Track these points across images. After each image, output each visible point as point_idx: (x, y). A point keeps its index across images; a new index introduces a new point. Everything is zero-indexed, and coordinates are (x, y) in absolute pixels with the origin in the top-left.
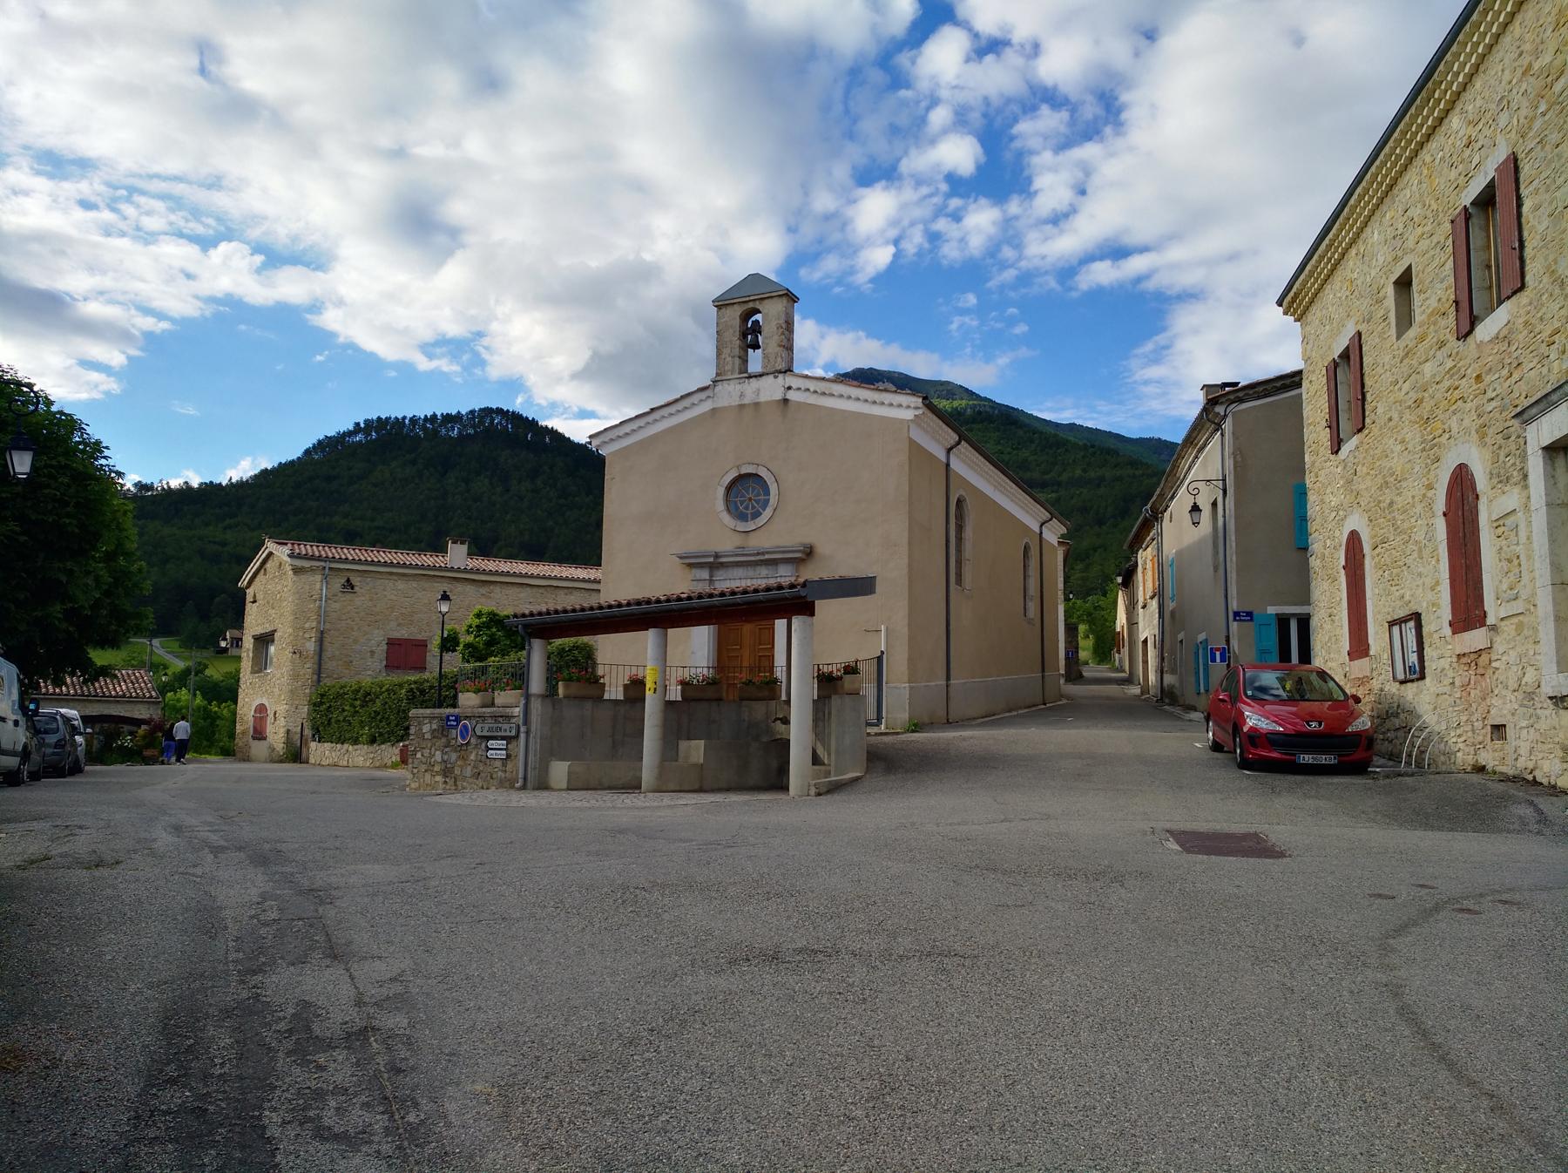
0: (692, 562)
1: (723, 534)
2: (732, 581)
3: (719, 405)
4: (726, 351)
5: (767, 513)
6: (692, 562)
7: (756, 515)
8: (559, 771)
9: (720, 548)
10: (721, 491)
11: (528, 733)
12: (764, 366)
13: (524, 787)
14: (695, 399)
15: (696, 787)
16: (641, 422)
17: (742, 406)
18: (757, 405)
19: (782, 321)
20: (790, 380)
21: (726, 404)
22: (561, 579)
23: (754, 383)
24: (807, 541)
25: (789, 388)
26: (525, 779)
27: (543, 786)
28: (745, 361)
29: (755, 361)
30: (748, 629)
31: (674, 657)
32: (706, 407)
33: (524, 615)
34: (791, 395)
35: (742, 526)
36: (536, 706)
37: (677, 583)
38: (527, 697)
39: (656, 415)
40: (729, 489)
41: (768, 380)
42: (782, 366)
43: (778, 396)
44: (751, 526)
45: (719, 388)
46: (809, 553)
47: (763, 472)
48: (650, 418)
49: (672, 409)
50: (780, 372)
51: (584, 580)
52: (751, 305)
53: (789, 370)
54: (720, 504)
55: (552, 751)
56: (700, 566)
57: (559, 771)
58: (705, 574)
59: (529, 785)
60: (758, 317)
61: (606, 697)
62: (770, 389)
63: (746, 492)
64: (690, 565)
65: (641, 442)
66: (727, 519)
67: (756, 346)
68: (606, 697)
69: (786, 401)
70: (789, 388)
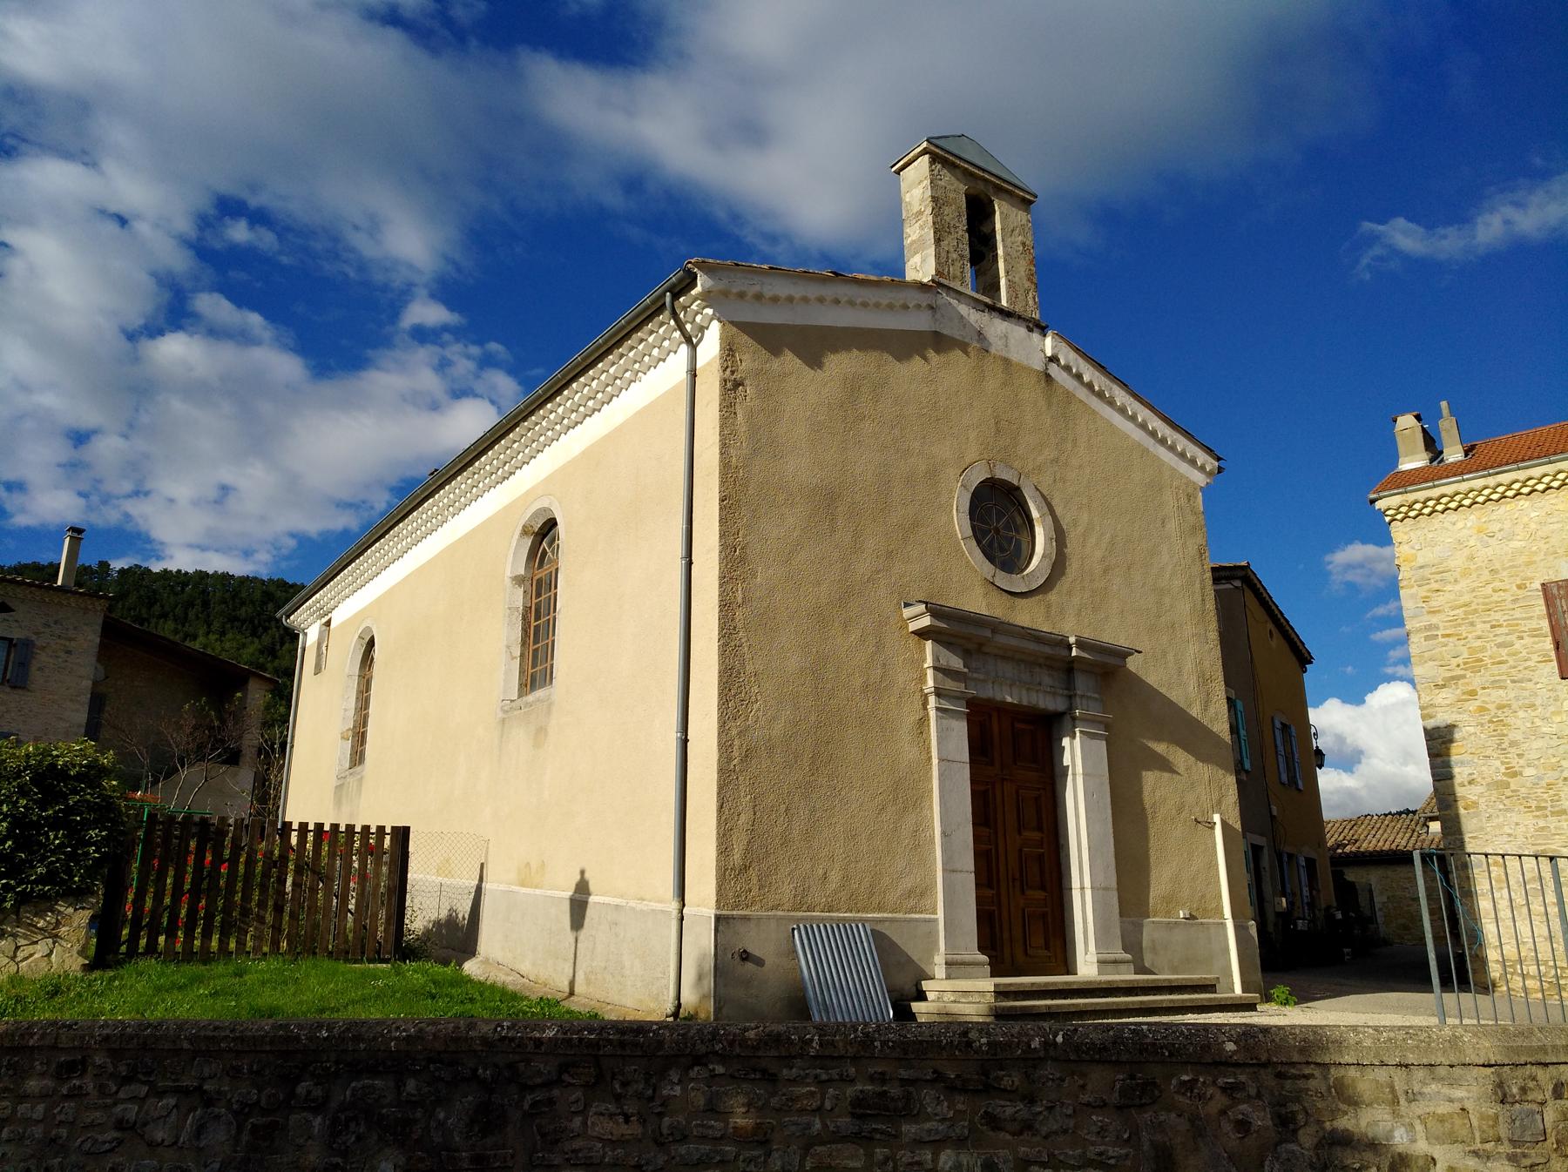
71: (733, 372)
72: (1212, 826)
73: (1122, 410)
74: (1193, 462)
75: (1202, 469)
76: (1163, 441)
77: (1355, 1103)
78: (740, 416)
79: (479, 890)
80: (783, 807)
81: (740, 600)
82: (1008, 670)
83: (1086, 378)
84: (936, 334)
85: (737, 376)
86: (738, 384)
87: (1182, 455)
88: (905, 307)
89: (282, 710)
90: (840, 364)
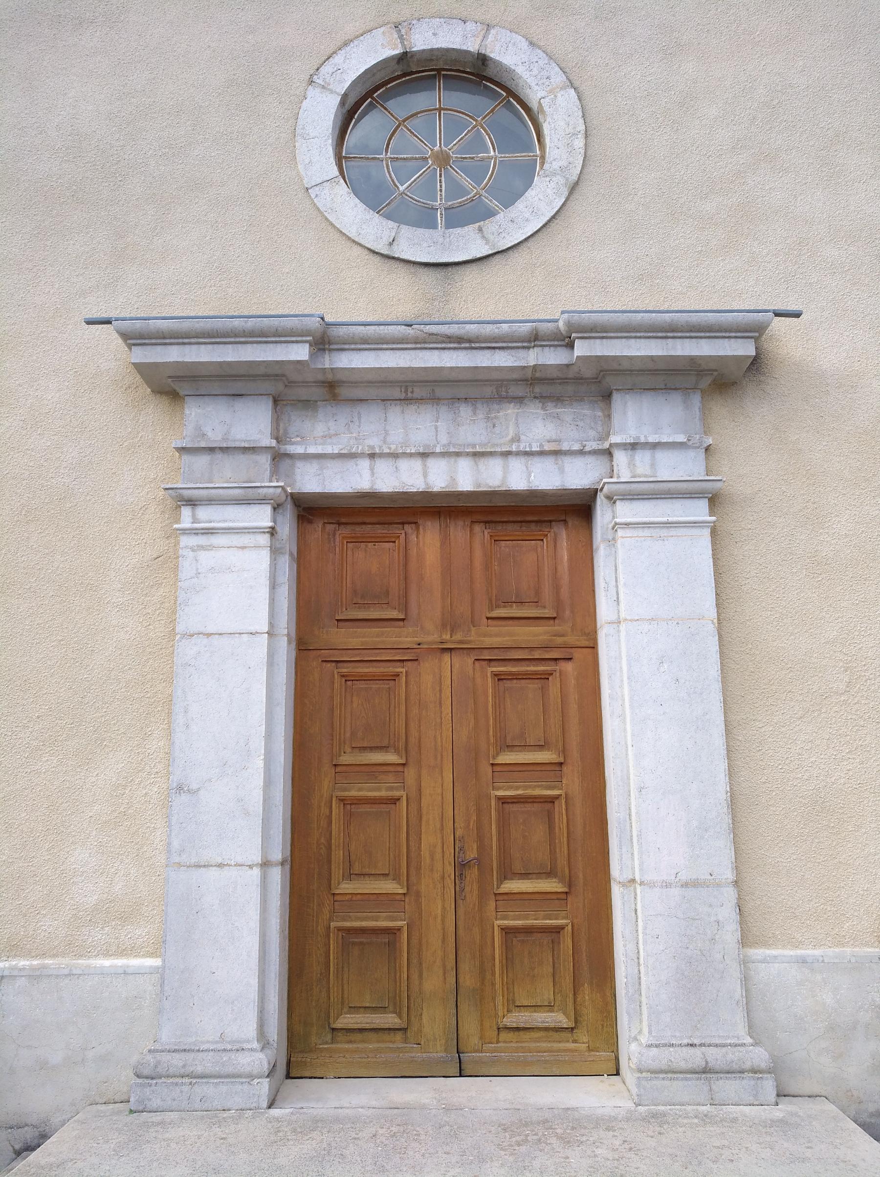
10: (321, 111)
35: (417, 245)
40: (351, 112)
44: (468, 243)
54: (317, 156)
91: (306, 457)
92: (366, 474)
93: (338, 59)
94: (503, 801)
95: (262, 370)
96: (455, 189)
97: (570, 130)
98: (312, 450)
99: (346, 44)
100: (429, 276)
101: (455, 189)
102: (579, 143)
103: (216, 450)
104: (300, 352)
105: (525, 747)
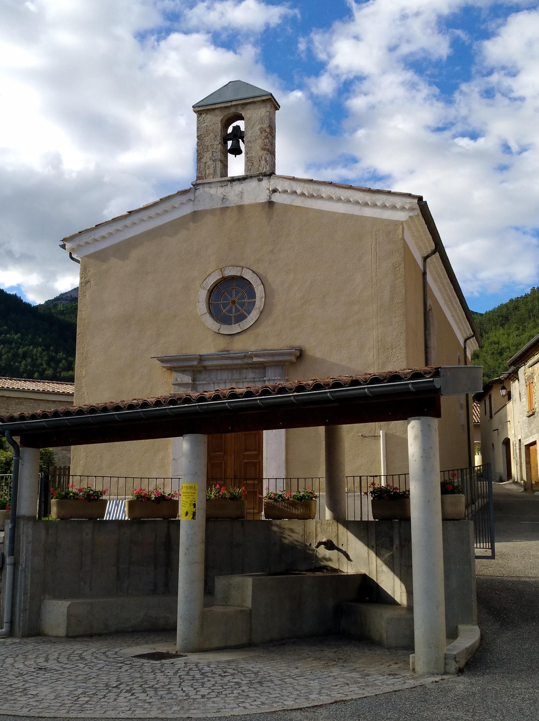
0: (175, 364)
1: (205, 337)
2: (215, 386)
3: (200, 208)
4: (207, 156)
5: (254, 316)
6: (175, 364)
7: (241, 318)
8: (57, 612)
9: (204, 351)
10: (203, 295)
11: (15, 565)
12: (247, 169)
13: (11, 634)
14: (176, 202)
15: (244, 640)
16: (119, 225)
17: (224, 210)
18: (240, 208)
19: (265, 125)
20: (273, 183)
21: (207, 207)
22: (13, 390)
23: (238, 187)
24: (298, 343)
25: (275, 191)
26: (12, 623)
27: (35, 632)
28: (225, 166)
29: (236, 166)
30: (231, 439)
31: (352, 465)
32: (187, 210)
33: (12, 419)
34: (276, 198)
35: (226, 329)
36: (26, 532)
37: (161, 387)
38: (15, 519)
39: (135, 218)
40: (211, 292)
41: (253, 184)
42: (266, 169)
43: (263, 198)
44: (236, 328)
45: (201, 190)
46: (300, 355)
47: (248, 275)
48: (128, 222)
49: (152, 212)
50: (265, 175)
51: (33, 391)
52: (233, 110)
53: (271, 174)
54: (202, 307)
55: (48, 586)
56: (182, 370)
57: (57, 612)
58: (187, 379)
59: (17, 629)
60: (241, 124)
61: (106, 517)
62: (256, 193)
63: (230, 297)
64: (171, 369)
65: (118, 245)
66: (210, 322)
67: (236, 151)
68: (106, 517)
69: (271, 204)
70: (275, 191)
71: (85, 278)
72: (377, 437)
73: (330, 198)
74: (394, 207)
75: (403, 209)
76: (366, 204)
77: (403, 83)
78: (87, 296)
79: (253, 272)
80: (99, 456)
81: (84, 375)
82: (225, 375)
83: (299, 192)
84: (195, 212)
85: (87, 279)
86: (87, 282)
87: (384, 207)
88: (174, 208)
89: (49, 372)
90: (135, 254)
91: (199, 384)
92: (213, 387)
93: (207, 280)
94: (246, 463)
95: (78, 639)
96: (237, 310)
97: (261, 296)
98: (200, 383)
99: (209, 275)
100: (227, 337)
101: (237, 310)
102: (263, 300)
103: (409, 376)
104: (195, 363)
105: (251, 450)
